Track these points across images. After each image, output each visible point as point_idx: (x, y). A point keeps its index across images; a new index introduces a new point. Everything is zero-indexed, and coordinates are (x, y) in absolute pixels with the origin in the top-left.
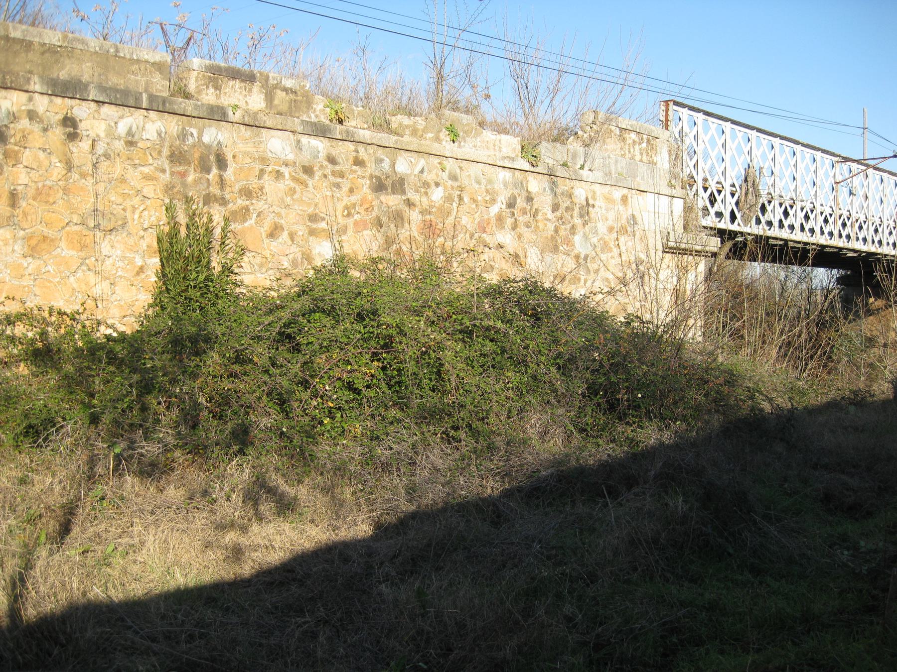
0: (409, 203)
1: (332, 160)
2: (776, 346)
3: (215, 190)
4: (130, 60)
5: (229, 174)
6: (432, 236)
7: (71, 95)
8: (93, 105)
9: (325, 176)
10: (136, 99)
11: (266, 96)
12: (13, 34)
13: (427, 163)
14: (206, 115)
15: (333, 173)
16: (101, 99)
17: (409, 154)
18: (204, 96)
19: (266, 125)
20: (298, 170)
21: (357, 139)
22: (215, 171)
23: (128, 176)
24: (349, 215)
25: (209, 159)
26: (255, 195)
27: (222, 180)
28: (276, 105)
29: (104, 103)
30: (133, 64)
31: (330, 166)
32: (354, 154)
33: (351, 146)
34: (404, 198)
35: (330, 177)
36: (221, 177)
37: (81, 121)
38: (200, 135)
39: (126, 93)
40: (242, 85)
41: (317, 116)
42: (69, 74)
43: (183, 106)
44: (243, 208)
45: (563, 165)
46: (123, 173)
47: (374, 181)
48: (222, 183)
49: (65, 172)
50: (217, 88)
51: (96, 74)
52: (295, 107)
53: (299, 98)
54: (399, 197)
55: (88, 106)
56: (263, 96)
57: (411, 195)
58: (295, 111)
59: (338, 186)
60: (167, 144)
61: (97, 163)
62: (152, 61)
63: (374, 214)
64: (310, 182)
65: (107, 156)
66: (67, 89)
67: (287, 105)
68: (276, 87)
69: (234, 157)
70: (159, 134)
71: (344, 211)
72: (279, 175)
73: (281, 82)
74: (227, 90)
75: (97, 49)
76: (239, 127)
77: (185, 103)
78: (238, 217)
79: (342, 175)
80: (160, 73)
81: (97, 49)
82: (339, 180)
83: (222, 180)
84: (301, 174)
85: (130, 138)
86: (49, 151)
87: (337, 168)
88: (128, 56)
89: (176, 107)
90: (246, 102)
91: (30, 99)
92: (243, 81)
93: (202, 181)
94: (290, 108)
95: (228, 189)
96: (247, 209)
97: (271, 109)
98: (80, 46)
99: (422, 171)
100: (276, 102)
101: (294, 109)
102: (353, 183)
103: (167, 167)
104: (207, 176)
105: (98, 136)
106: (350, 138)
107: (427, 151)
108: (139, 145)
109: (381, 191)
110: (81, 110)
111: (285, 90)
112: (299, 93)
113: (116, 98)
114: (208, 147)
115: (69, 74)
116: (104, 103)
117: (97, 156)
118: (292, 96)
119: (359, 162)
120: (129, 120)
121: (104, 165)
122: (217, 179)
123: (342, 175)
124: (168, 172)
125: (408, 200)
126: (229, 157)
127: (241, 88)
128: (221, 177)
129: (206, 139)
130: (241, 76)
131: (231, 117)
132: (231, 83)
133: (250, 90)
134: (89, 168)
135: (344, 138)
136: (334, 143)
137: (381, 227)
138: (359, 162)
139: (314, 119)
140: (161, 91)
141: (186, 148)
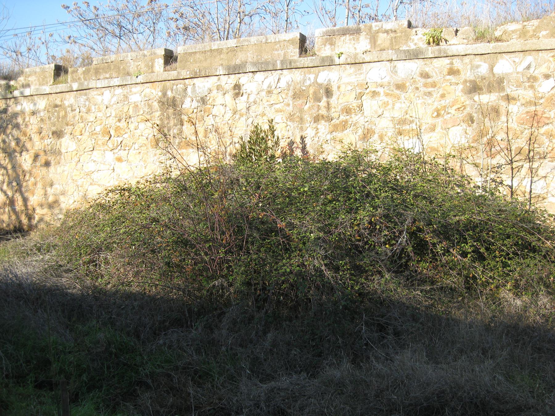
0: (508, 99)
1: (425, 75)
2: (405, 210)
3: (323, 112)
4: (275, 42)
5: (333, 101)
6: (535, 125)
7: (237, 72)
8: (251, 74)
9: (417, 88)
10: (273, 65)
11: (370, 41)
12: (214, 48)
13: (535, 59)
14: (318, 64)
15: (425, 85)
16: (253, 70)
17: (513, 55)
18: (322, 52)
19: (364, 61)
20: (392, 88)
21: (450, 54)
22: (325, 99)
23: (266, 112)
24: (438, 115)
25: (320, 92)
26: (353, 111)
27: (328, 104)
28: (379, 45)
29: (256, 72)
30: (276, 45)
31: (423, 80)
32: (448, 66)
33: (447, 61)
34: (502, 95)
35: (422, 89)
36: (328, 104)
37: (243, 85)
38: (316, 78)
39: (267, 63)
40: (351, 37)
41: (416, 44)
42: (241, 61)
43: (302, 62)
44: (343, 121)
45: (450, 93)
46: (264, 111)
47: (468, 84)
48: (328, 107)
49: (232, 115)
50: (332, 44)
51: (255, 56)
52: (395, 42)
53: (398, 35)
54: (497, 94)
55: (248, 76)
56: (368, 41)
57: (510, 90)
58: (396, 45)
59: (430, 94)
60: (291, 88)
61: (249, 107)
62: (287, 40)
63: (465, 112)
64: (403, 95)
65: (255, 102)
66: (235, 69)
67: (389, 42)
68: (378, 32)
69: (339, 87)
70: (288, 83)
71: (433, 114)
72: (375, 94)
73: (382, 27)
74: (339, 44)
75: (256, 42)
76: (345, 67)
77: (304, 60)
78: (339, 128)
79: (434, 85)
80: (293, 45)
81: (256, 42)
82: (430, 89)
83: (328, 104)
84: (395, 91)
85: (269, 89)
86: (225, 105)
87: (429, 80)
88: (273, 41)
89: (298, 64)
90: (355, 48)
91: (219, 79)
92: (351, 34)
93: (314, 108)
94: (391, 43)
95: (333, 110)
96: (346, 122)
97: (375, 48)
98: (246, 43)
99: (528, 67)
100: (379, 42)
101: (394, 44)
102: (445, 90)
103: (291, 102)
104: (319, 104)
105: (251, 91)
106: (442, 55)
107: (534, 48)
108: (274, 92)
109: (475, 92)
110: (244, 79)
111: (387, 32)
112: (398, 31)
113: (262, 67)
114: (320, 85)
115: (241, 61)
116: (256, 72)
117: (250, 103)
118: (393, 35)
119: (453, 72)
120: (272, 77)
121: (253, 108)
122: (325, 104)
123: (434, 85)
124: (291, 105)
125: (508, 95)
126: (334, 89)
127: (350, 40)
128: (328, 104)
129: (320, 81)
130: (350, 31)
131: (337, 61)
132: (343, 38)
133: (358, 39)
134: (244, 111)
135: (436, 56)
136: (428, 62)
137: (473, 122)
138: (453, 72)
139: (413, 47)
140: (293, 56)
141: (304, 88)
